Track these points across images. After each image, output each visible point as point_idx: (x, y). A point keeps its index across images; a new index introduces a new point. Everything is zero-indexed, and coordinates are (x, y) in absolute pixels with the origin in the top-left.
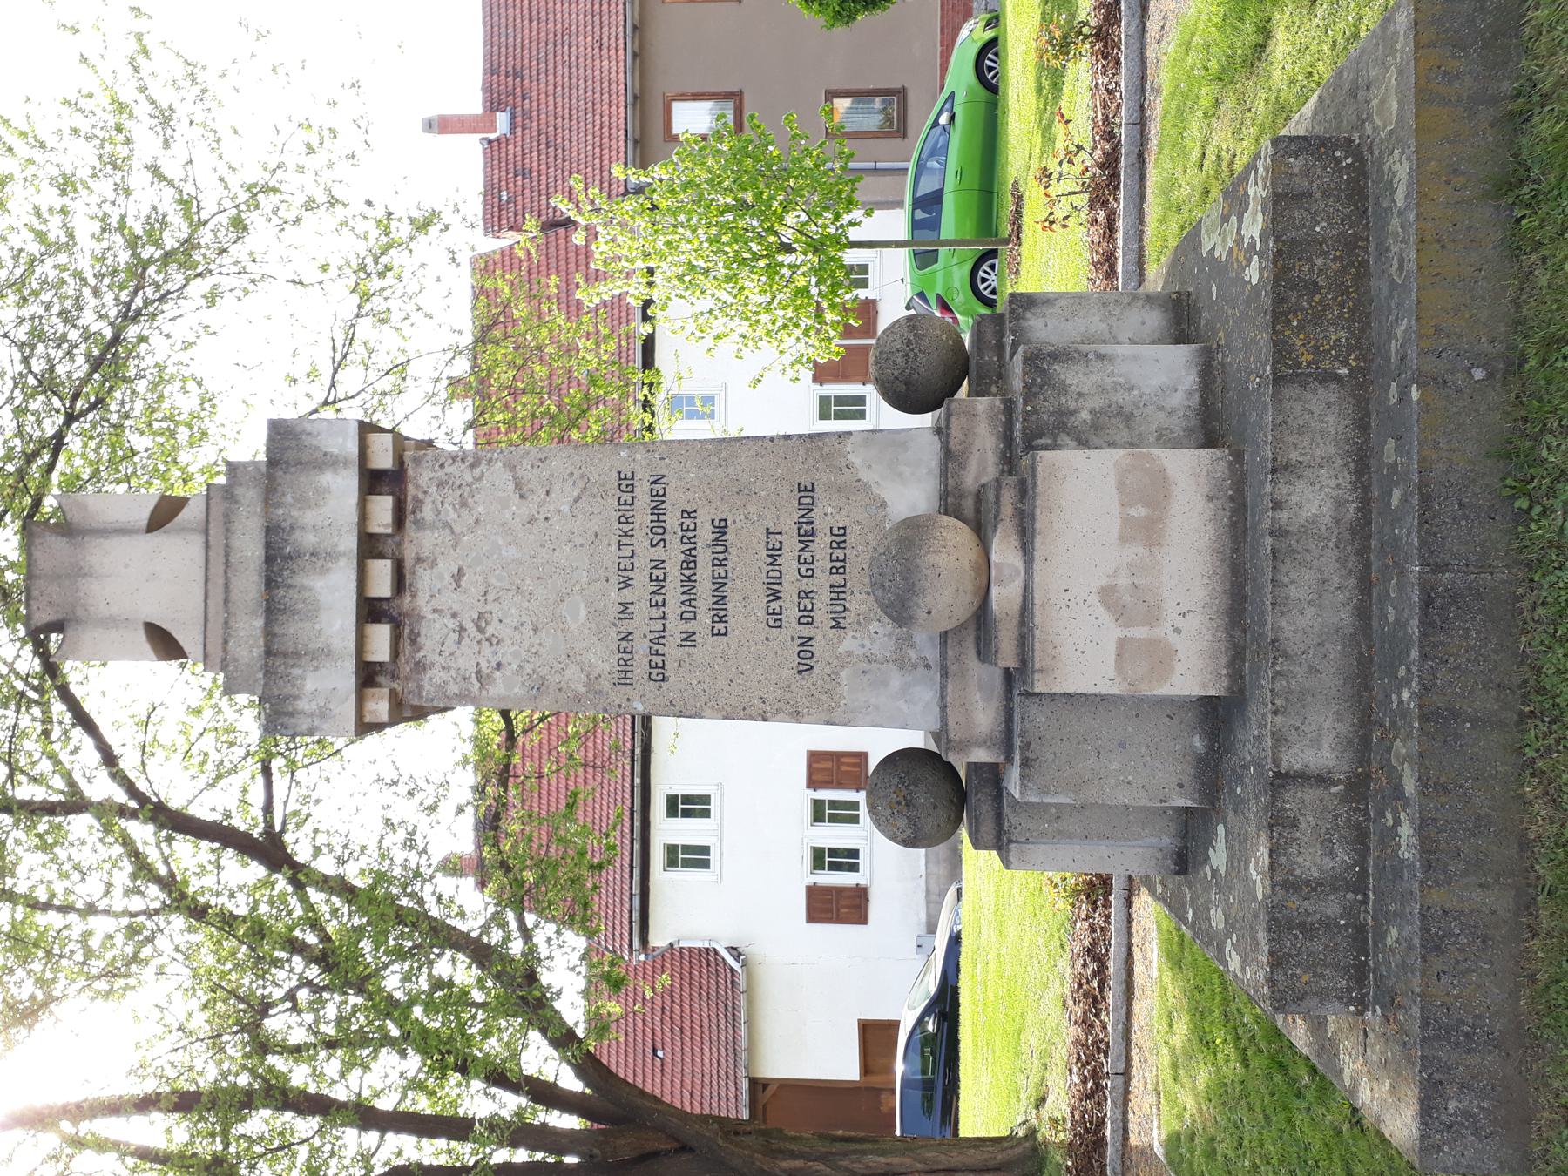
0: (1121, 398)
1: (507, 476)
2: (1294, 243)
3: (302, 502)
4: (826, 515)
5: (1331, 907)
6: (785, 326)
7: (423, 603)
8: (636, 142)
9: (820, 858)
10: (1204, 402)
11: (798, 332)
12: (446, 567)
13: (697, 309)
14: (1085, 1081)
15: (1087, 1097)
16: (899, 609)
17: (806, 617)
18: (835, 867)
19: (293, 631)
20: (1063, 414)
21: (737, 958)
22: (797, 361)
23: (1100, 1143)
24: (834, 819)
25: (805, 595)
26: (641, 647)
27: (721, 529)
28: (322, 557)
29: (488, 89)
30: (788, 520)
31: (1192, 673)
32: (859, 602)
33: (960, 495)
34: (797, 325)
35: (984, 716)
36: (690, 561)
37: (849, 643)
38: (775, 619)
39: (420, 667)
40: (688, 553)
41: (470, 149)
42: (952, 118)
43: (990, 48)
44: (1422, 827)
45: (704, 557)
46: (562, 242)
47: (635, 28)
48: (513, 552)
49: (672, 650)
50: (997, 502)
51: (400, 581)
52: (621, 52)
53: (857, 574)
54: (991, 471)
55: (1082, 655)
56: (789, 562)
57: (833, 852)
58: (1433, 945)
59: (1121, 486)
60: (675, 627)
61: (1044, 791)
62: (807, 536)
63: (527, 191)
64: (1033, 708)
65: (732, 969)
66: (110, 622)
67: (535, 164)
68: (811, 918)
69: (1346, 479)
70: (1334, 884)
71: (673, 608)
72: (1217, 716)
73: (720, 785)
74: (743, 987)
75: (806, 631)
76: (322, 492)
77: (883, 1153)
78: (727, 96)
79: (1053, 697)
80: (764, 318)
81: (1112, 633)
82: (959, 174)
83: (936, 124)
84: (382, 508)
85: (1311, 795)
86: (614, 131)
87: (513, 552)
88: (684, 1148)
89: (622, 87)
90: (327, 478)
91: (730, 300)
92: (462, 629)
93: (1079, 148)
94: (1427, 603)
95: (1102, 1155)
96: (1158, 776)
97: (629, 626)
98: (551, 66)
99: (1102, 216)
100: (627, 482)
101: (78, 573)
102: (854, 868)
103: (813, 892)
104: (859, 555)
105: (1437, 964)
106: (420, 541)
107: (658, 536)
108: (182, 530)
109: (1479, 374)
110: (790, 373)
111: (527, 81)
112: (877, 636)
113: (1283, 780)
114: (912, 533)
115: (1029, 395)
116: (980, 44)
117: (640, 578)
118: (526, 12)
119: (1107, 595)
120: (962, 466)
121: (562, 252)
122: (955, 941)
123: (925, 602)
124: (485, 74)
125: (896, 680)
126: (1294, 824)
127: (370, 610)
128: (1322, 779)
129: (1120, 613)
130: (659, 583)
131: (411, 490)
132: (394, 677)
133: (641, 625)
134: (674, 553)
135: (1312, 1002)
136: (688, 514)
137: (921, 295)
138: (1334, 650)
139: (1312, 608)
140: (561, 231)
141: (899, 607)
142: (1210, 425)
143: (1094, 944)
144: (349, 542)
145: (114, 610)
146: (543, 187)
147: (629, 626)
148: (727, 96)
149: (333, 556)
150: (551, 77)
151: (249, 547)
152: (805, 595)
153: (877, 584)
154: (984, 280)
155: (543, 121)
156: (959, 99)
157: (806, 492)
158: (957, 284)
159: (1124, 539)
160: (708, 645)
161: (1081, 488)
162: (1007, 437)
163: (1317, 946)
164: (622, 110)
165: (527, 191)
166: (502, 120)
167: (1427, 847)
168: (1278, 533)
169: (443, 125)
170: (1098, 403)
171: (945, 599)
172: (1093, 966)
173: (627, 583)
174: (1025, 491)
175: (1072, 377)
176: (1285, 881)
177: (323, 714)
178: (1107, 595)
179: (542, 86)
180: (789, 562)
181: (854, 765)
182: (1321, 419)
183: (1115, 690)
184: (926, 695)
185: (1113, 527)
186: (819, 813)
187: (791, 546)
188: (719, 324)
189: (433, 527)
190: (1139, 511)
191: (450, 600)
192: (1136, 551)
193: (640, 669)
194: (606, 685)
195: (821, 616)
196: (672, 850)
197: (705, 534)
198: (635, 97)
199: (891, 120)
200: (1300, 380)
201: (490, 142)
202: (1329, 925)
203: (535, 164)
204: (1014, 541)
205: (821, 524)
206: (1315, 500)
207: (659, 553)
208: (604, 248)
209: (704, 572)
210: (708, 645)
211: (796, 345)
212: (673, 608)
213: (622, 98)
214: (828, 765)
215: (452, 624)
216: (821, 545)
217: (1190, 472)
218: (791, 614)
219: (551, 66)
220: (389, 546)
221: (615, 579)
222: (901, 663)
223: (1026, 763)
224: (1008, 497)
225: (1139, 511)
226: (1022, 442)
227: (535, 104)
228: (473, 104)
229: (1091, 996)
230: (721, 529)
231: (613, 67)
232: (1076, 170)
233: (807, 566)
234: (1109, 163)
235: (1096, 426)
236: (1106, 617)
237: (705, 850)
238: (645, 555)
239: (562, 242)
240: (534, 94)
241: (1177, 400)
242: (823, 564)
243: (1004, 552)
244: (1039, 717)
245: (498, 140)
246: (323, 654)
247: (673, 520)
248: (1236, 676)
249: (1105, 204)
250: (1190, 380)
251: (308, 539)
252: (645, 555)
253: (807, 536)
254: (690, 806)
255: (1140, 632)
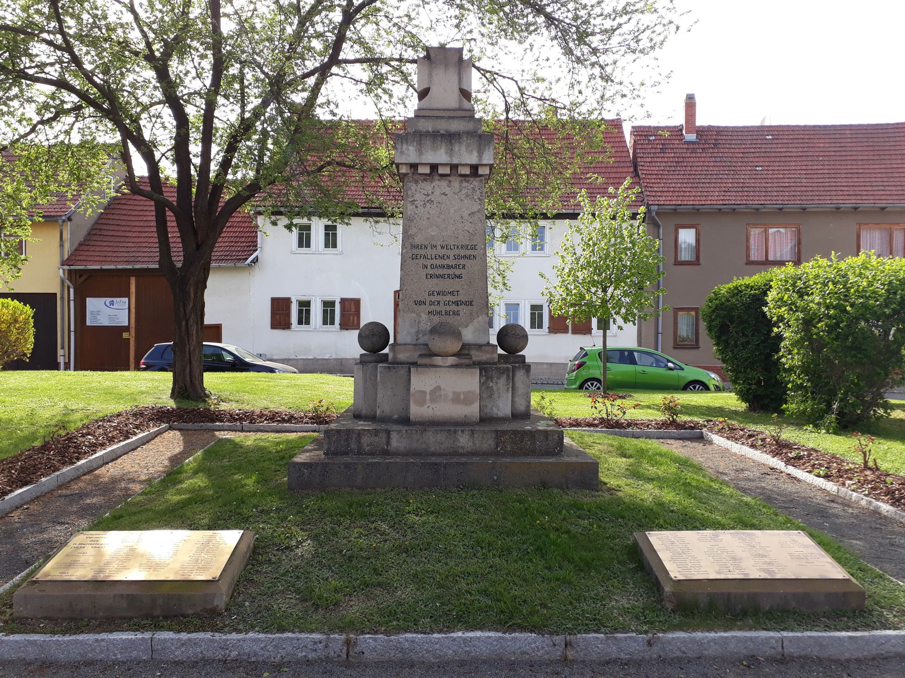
0: (496, 394)
1: (476, 210)
2: (534, 436)
3: (468, 146)
4: (464, 310)
5: (353, 446)
6: (567, 289)
7: (436, 183)
8: (675, 210)
9: (305, 306)
10: (495, 418)
11: (564, 296)
12: (448, 190)
13: (576, 247)
14: (237, 415)
15: (231, 416)
16: (434, 331)
17: (432, 303)
18: (300, 312)
19: (428, 143)
20: (492, 378)
21: (253, 262)
22: (551, 295)
23: (213, 421)
24: (325, 312)
25: (439, 303)
26: (422, 252)
27: (459, 277)
28: (450, 152)
29: (710, 129)
30: (462, 298)
31: (416, 411)
32: (436, 319)
33: (469, 350)
34: (567, 295)
35: (402, 356)
36: (449, 267)
37: (423, 316)
38: (431, 294)
39: (416, 182)
40: (452, 266)
41: (678, 119)
42: (671, 369)
43: (706, 388)
44: (379, 463)
45: (451, 271)
46: (626, 170)
47: (734, 209)
48: (452, 212)
49: (422, 261)
50: (465, 356)
51: (443, 176)
52: (721, 202)
53: (444, 318)
54: (475, 359)
55: (421, 382)
56: (449, 298)
57: (308, 312)
58: (347, 466)
59: (470, 392)
60: (429, 263)
61: (381, 373)
62: (457, 303)
63: (654, 151)
64: (406, 370)
65: (247, 259)
66: (430, 76)
67: (668, 155)
68: (274, 301)
69: (469, 449)
70: (360, 446)
71: (435, 262)
72: (405, 421)
73: (342, 253)
74: (238, 265)
75: (427, 303)
76: (471, 152)
77: (197, 333)
78: (698, 258)
79: (409, 375)
80: (571, 278)
81: (428, 389)
82: (644, 373)
83: (669, 361)
84: (467, 171)
85: (384, 440)
86: (681, 198)
87: (452, 212)
88: (198, 247)
89: (703, 203)
90: (475, 154)
91: (580, 263)
92: (428, 195)
93: (624, 413)
94: (436, 464)
95: (208, 422)
96: (385, 404)
97: (429, 248)
98: (718, 164)
99: (596, 422)
100: (474, 247)
101: (446, 66)
102: (300, 322)
103: (287, 301)
104: (451, 320)
105: (342, 467)
106: (456, 183)
107: (456, 257)
108: (460, 101)
109: (495, 478)
110: (546, 292)
111: (711, 150)
112: (426, 325)
113: (388, 433)
114: (458, 335)
115: (497, 369)
116: (707, 382)
117: (444, 252)
118: (748, 150)
119: (438, 388)
120: (477, 350)
121: (621, 170)
122: (271, 370)
123: (437, 338)
124: (718, 127)
125: (413, 331)
126: (376, 436)
127: (434, 167)
128: (388, 443)
129: (433, 392)
130: (443, 257)
131: (472, 179)
132: (413, 174)
133: (430, 252)
134: (452, 262)
135: (327, 441)
136: (464, 266)
137: (586, 355)
138: (423, 446)
139: (435, 440)
140: (632, 169)
141: (435, 331)
142: (485, 419)
143: (295, 418)
144: (455, 161)
145: (434, 77)
146: (656, 159)
147: (429, 248)
148: (698, 258)
149: (451, 156)
150: (712, 164)
151: (455, 126)
152: (439, 303)
153: (441, 324)
154: (592, 384)
155: (690, 160)
156: (680, 373)
157: (471, 303)
158: (591, 371)
159: (454, 393)
160: (424, 272)
161: (470, 381)
162: (486, 363)
163: (342, 442)
164: (691, 203)
165: (654, 151)
166: (692, 137)
167: (373, 464)
168: (455, 432)
169: (690, 104)
170: (495, 388)
171: (437, 344)
172: (286, 418)
173: (442, 247)
174: (468, 366)
175: (503, 381)
176: (360, 434)
177: (402, 153)
178: (438, 388)
179: (709, 159)
180: (449, 298)
181: (353, 323)
182: (486, 442)
183: (411, 390)
184: (408, 340)
185: (458, 390)
186: (328, 305)
187: (454, 299)
188: (569, 258)
189: (460, 186)
190: (462, 397)
191: (437, 192)
192: (451, 396)
193: (416, 251)
194: (411, 241)
195: (433, 308)
196: (308, 228)
197: (458, 272)
198: (698, 210)
199: (683, 341)
200: (497, 437)
201: (681, 130)
202: (349, 445)
203: (668, 155)
204: (454, 363)
205: (460, 308)
206: (464, 441)
207: (452, 258)
208: (605, 203)
209: (446, 271)
210: (424, 272)
211: (559, 293)
212: (435, 262)
213: (697, 203)
214: (353, 309)
215: (430, 192)
216: (454, 308)
217: (473, 410)
218: (433, 299)
219: (718, 164)
220: (454, 172)
221: (444, 244)
222: (418, 332)
223: (389, 368)
224: (467, 361)
225: (462, 397)
226: (485, 369)
227: (699, 155)
228: (701, 120)
229: (273, 417)
230: (459, 277)
231: (715, 198)
232: (615, 412)
233: (448, 303)
234: (618, 425)
235: (488, 387)
236: (432, 388)
237: (308, 245)
238: (451, 253)
239: (626, 170)
240: (704, 155)
241: (495, 411)
242: (448, 308)
243: (451, 360)
244: (403, 372)
245: (682, 135)
246: (420, 152)
247: (462, 262)
248: (416, 423)
249: (601, 423)
250: (501, 414)
251: (456, 148)
252: (451, 253)
253: (457, 303)
254: (331, 240)
255: (428, 397)
